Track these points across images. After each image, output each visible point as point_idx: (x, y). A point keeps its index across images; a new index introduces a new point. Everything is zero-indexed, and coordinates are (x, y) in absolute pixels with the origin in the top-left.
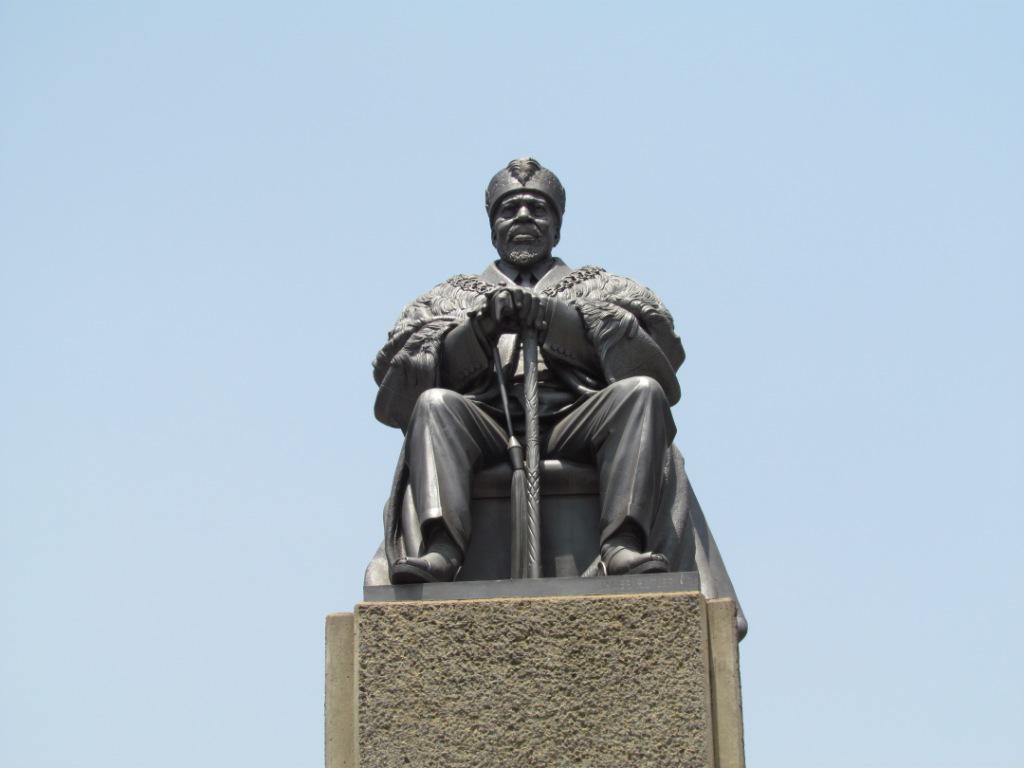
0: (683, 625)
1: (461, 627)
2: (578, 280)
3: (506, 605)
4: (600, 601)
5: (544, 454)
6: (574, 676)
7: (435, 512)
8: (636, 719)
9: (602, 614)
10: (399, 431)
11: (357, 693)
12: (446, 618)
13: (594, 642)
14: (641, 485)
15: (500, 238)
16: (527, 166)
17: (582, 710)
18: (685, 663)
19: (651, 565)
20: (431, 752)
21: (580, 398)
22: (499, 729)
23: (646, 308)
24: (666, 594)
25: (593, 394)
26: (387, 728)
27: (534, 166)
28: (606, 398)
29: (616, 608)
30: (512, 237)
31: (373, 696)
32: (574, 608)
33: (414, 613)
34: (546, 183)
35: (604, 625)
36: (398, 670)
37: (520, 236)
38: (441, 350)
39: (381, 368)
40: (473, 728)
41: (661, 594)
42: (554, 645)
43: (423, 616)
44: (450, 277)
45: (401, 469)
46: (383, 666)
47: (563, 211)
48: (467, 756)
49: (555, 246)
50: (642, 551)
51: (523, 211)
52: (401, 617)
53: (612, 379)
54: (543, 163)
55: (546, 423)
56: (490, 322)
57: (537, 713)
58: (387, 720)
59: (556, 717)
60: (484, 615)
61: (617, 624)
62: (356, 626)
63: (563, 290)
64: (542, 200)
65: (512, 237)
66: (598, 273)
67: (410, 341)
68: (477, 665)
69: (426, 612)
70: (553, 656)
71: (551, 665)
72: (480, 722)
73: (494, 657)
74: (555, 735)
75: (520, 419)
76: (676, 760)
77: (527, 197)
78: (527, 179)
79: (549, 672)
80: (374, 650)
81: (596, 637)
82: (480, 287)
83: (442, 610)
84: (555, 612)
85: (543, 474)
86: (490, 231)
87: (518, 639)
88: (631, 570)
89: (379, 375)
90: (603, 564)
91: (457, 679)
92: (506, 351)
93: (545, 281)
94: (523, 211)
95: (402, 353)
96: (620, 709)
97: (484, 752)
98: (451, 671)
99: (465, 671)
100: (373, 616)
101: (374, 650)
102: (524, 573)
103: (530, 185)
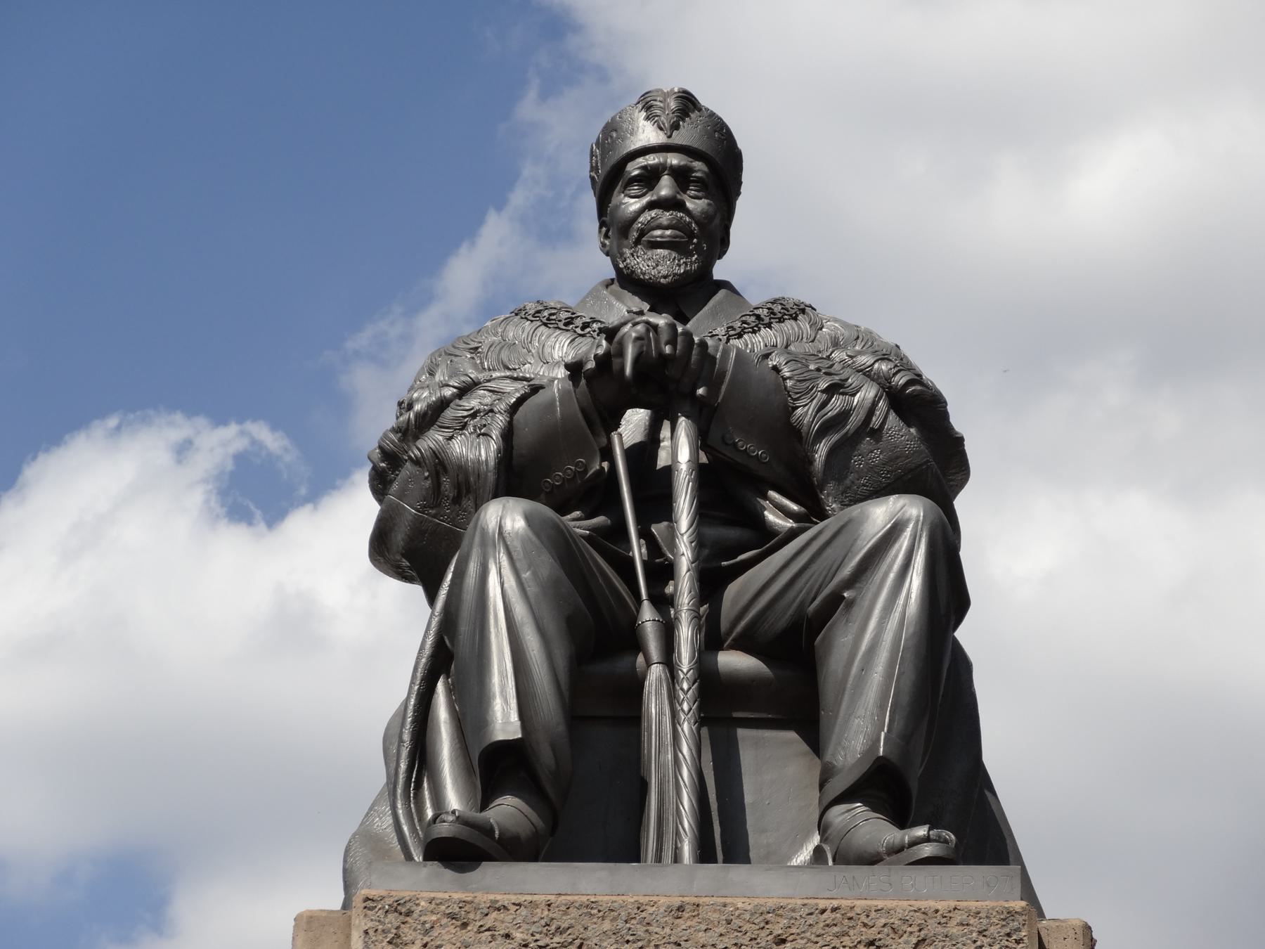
2: (767, 320)
3: (651, 910)
4: (834, 910)
5: (711, 640)
12: (534, 929)
14: (905, 699)
16: (673, 105)
19: (927, 850)
21: (768, 540)
23: (900, 380)
24: (963, 904)
25: (792, 535)
27: (687, 103)
28: (828, 543)
29: (865, 925)
30: (642, 233)
33: (471, 916)
34: (710, 136)
37: (658, 232)
38: (508, 434)
41: (953, 904)
43: (489, 922)
45: (428, 651)
47: (738, 193)
49: (720, 257)
50: (902, 821)
52: (444, 921)
53: (639, 527)
54: (703, 100)
60: (607, 925)
63: (740, 336)
64: (698, 165)
65: (642, 233)
66: (803, 311)
67: (449, 413)
69: (494, 915)
75: (662, 571)
77: (674, 160)
78: (675, 127)
82: (579, 322)
83: (523, 911)
84: (746, 927)
85: (707, 678)
86: (732, 230)
90: (827, 848)
92: (685, 447)
94: (665, 188)
95: (433, 439)
100: (391, 917)
102: (667, 855)
103: (679, 138)
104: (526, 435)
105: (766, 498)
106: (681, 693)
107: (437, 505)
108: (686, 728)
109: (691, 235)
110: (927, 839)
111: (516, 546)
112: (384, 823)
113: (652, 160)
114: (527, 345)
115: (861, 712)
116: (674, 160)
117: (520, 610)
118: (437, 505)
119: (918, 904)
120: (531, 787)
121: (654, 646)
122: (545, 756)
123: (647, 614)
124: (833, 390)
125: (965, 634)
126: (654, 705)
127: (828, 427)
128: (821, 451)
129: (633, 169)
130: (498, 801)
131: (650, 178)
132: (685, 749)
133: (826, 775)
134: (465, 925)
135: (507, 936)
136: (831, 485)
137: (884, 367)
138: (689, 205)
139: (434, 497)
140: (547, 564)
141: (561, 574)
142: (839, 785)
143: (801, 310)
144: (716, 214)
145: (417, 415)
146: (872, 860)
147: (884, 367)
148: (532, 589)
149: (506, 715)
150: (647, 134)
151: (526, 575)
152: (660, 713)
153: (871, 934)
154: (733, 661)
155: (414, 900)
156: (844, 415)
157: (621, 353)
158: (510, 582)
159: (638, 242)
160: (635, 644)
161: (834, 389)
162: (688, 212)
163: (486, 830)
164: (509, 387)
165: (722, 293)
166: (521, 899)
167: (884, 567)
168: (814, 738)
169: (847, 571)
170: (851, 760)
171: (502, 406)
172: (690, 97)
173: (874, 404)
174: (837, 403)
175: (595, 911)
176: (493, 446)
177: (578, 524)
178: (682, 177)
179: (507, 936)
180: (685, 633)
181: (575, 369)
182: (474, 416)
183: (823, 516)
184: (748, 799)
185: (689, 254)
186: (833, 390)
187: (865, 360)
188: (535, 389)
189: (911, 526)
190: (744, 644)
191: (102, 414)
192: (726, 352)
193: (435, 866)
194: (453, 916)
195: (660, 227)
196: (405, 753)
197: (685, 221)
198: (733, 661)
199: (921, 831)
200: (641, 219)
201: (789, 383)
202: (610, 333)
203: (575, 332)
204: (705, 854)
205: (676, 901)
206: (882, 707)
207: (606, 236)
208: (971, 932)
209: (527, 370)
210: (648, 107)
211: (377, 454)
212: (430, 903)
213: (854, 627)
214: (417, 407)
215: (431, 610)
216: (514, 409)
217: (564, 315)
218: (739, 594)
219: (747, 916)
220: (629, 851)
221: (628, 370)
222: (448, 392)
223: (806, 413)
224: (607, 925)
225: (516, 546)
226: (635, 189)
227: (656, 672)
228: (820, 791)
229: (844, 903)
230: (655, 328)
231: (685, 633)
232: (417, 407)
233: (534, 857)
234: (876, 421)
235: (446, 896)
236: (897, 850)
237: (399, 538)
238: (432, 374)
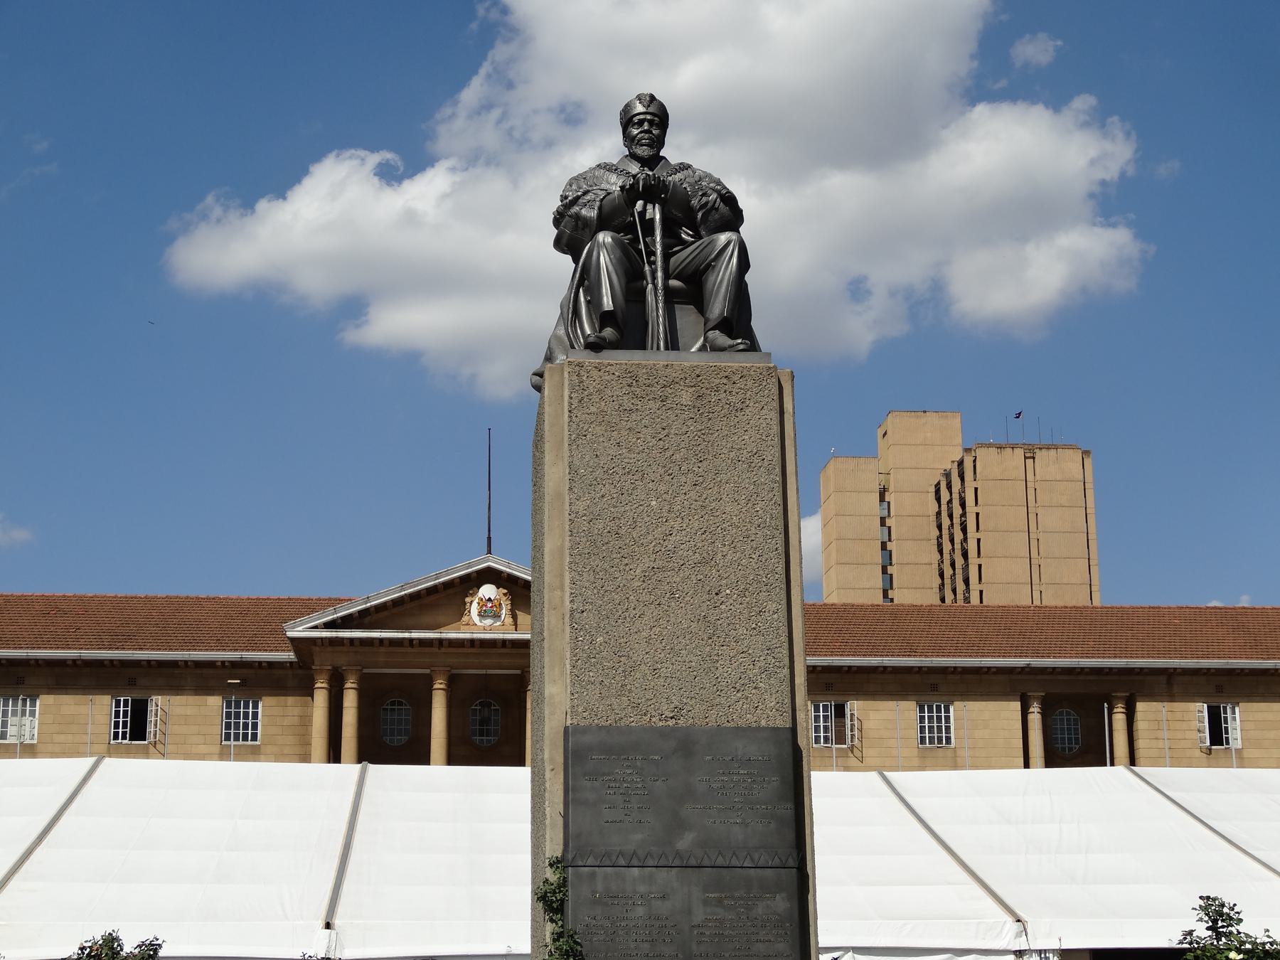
0: (764, 384)
1: (631, 377)
5: (667, 276)
6: (699, 411)
7: (607, 303)
8: (736, 439)
9: (716, 375)
10: (568, 258)
11: (566, 414)
13: (711, 391)
15: (629, 140)
17: (703, 432)
18: (765, 407)
19: (741, 347)
20: (611, 452)
21: (686, 244)
22: (654, 440)
23: (724, 192)
25: (693, 243)
26: (585, 436)
27: (652, 98)
31: (576, 416)
32: (700, 370)
35: (717, 381)
36: (592, 401)
37: (644, 141)
38: (600, 208)
39: (558, 220)
40: (638, 439)
42: (687, 391)
44: (598, 163)
46: (582, 399)
48: (633, 456)
50: (733, 337)
51: (646, 126)
53: (703, 233)
55: (667, 257)
56: (631, 193)
57: (676, 432)
58: (585, 431)
59: (688, 435)
60: (644, 371)
61: (725, 381)
62: (566, 375)
63: (671, 176)
64: (656, 118)
65: (639, 141)
67: (581, 201)
68: (640, 401)
70: (686, 397)
71: (685, 403)
72: (642, 436)
73: (651, 397)
74: (687, 446)
76: (760, 464)
77: (649, 117)
78: (649, 106)
79: (684, 408)
80: (577, 388)
81: (712, 387)
85: (666, 288)
87: (665, 386)
88: (729, 349)
89: (557, 222)
91: (628, 409)
93: (661, 167)
94: (646, 126)
95: (575, 209)
96: (726, 432)
97: (644, 454)
98: (625, 404)
99: (633, 404)
101: (577, 388)
103: (651, 110)
104: (606, 209)
105: (682, 229)
107: (576, 230)
108: (660, 305)
109: (654, 142)
110: (741, 343)
111: (609, 247)
112: (562, 332)
113: (642, 117)
114: (602, 178)
115: (717, 301)
116: (649, 117)
117: (611, 268)
118: (576, 230)
119: (741, 365)
120: (616, 326)
121: (649, 279)
122: (619, 314)
123: (647, 268)
124: (703, 195)
125: (748, 277)
126: (650, 298)
127: (702, 207)
128: (700, 215)
129: (636, 119)
130: (605, 329)
131: (641, 123)
132: (660, 311)
133: (706, 321)
134: (600, 370)
135: (613, 374)
136: (702, 226)
137: (719, 187)
138: (654, 132)
139: (576, 228)
140: (618, 252)
141: (622, 254)
142: (711, 324)
143: (688, 167)
145: (570, 201)
146: (722, 349)
147: (719, 187)
148: (614, 261)
149: (608, 302)
150: (640, 108)
151: (612, 257)
152: (652, 300)
153: (726, 374)
154: (674, 283)
155: (584, 362)
156: (707, 203)
157: (638, 183)
158: (607, 259)
159: (637, 144)
160: (643, 277)
161: (704, 195)
162: (653, 135)
163: (604, 339)
164: (600, 192)
165: (663, 161)
166: (617, 362)
167: (726, 253)
168: (701, 308)
169: (713, 256)
170: (714, 317)
171: (598, 199)
173: (716, 199)
174: (704, 199)
176: (596, 212)
177: (627, 238)
178: (651, 123)
179: (613, 374)
180: (660, 274)
181: (622, 188)
182: (588, 202)
183: (701, 238)
184: (678, 327)
185: (654, 148)
186: (703, 195)
187: (712, 185)
188: (609, 194)
190: (676, 278)
191: (330, 151)
192: (670, 182)
193: (588, 351)
194: (596, 367)
195: (645, 139)
196: (570, 311)
198: (674, 283)
199: (739, 341)
201: (690, 193)
202: (634, 176)
204: (667, 348)
205: (666, 363)
206: (725, 300)
207: (626, 141)
209: (604, 186)
210: (639, 99)
211: (556, 214)
212: (975, 480)
213: (715, 274)
214: (570, 198)
215: (574, 265)
216: (602, 200)
217: (614, 168)
218: (675, 262)
220: (642, 346)
221: (641, 189)
222: (579, 194)
223: (694, 202)
224: (644, 371)
225: (609, 247)
226: (636, 127)
227: (650, 286)
228: (705, 325)
229: (718, 364)
230: (649, 175)
231: (660, 274)
232: (570, 198)
233: (617, 348)
234: (717, 205)
235: (593, 361)
236: (731, 346)
237: (564, 240)
238: (571, 186)
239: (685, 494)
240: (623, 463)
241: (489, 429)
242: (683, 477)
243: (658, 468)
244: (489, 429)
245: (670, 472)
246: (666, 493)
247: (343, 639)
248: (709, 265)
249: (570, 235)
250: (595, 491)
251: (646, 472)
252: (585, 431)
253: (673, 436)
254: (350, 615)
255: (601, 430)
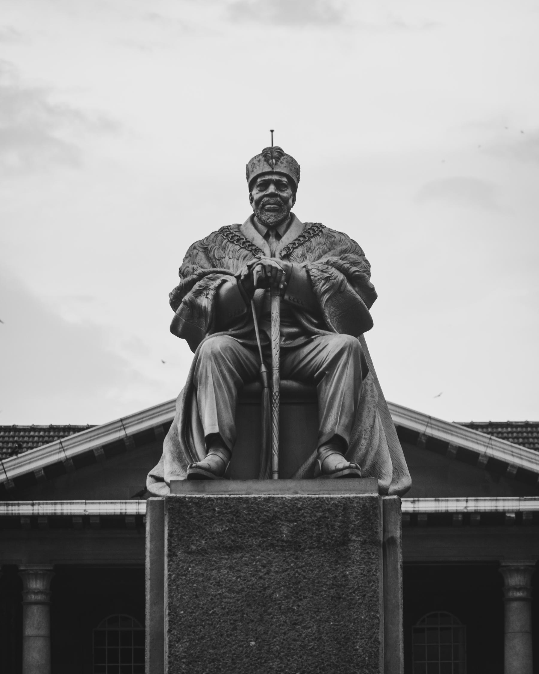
1: (231, 512)
10: (183, 343)
30: (264, 205)
33: (202, 503)
38: (217, 296)
43: (207, 505)
48: (233, 595)
54: (286, 152)
60: (245, 506)
72: (242, 574)
77: (275, 177)
79: (284, 544)
83: (219, 501)
89: (174, 304)
94: (272, 189)
106: (275, 396)
113: (267, 177)
144: (291, 197)
172: (281, 151)
175: (241, 501)
189: (348, 349)
197: (200, 573)
200: (263, 200)
203: (240, 246)
208: (360, 505)
219: (289, 502)
239: (285, 633)
240: (223, 603)
241: (272, 131)
242: (283, 616)
243: (257, 608)
244: (272, 131)
245: (270, 610)
246: (266, 633)
247: (18, 518)
248: (323, 374)
249: (185, 323)
250: (194, 632)
251: (246, 612)
252: (185, 571)
253: (273, 574)
254: (30, 475)
255: (201, 569)
